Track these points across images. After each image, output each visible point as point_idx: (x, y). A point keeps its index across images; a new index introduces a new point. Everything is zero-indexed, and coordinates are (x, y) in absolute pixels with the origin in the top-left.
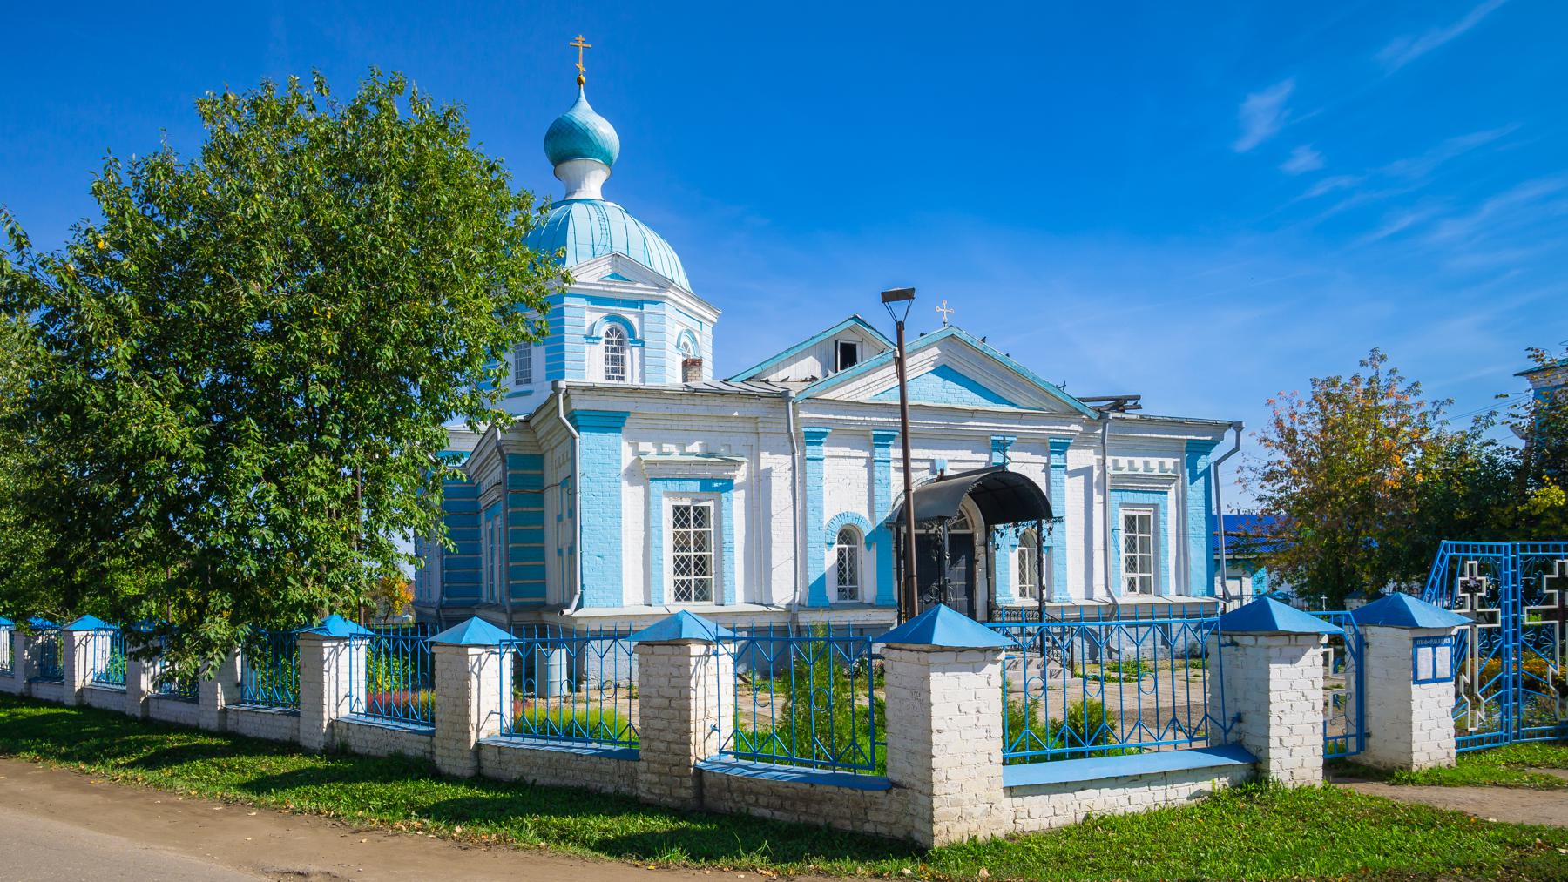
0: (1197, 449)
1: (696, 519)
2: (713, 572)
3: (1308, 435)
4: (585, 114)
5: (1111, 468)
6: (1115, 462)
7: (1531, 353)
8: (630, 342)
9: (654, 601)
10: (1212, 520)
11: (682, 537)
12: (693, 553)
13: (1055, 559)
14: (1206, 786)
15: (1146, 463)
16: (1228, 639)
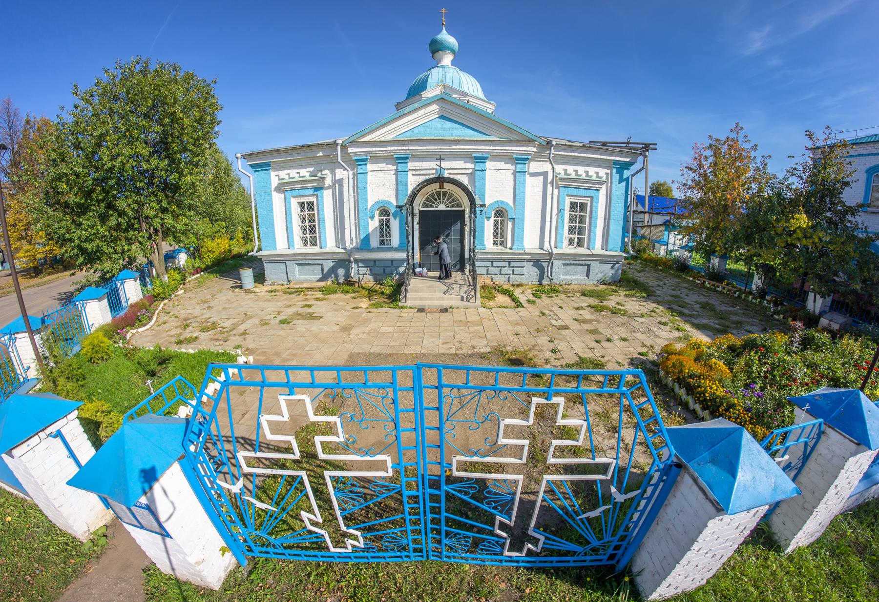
7: (807, 133)
12: (307, 224)
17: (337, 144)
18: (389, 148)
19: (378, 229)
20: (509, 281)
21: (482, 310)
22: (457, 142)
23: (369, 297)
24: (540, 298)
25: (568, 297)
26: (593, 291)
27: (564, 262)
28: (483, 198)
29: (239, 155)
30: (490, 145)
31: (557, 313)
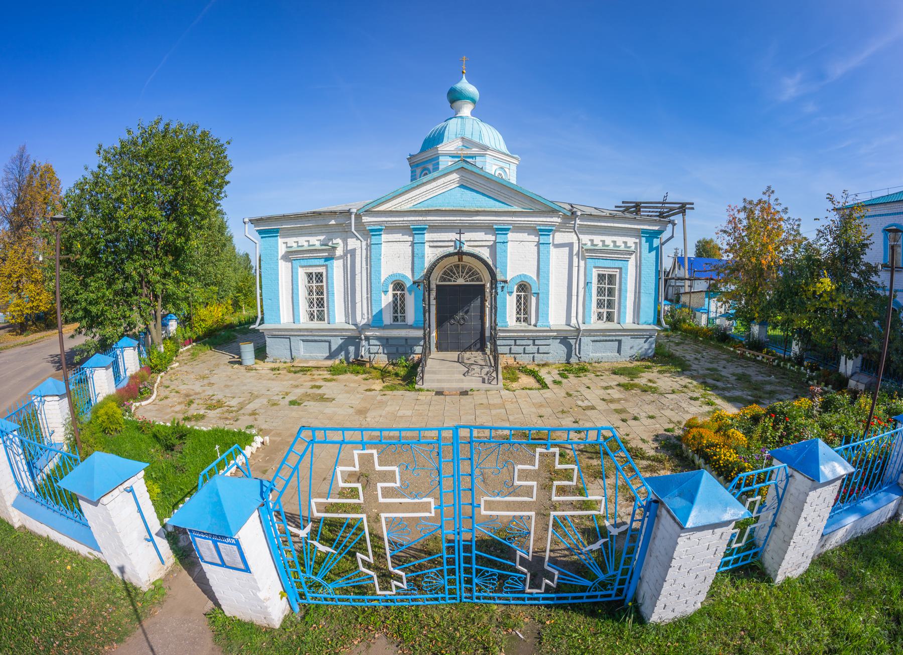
12: (314, 297)
17: (351, 214)
18: (406, 219)
19: (392, 303)
20: (534, 361)
21: (504, 393)
22: (477, 213)
23: (382, 379)
24: (566, 378)
25: (598, 376)
26: (625, 369)
27: (593, 338)
28: (505, 273)
29: (247, 220)
30: (512, 216)
31: (584, 394)
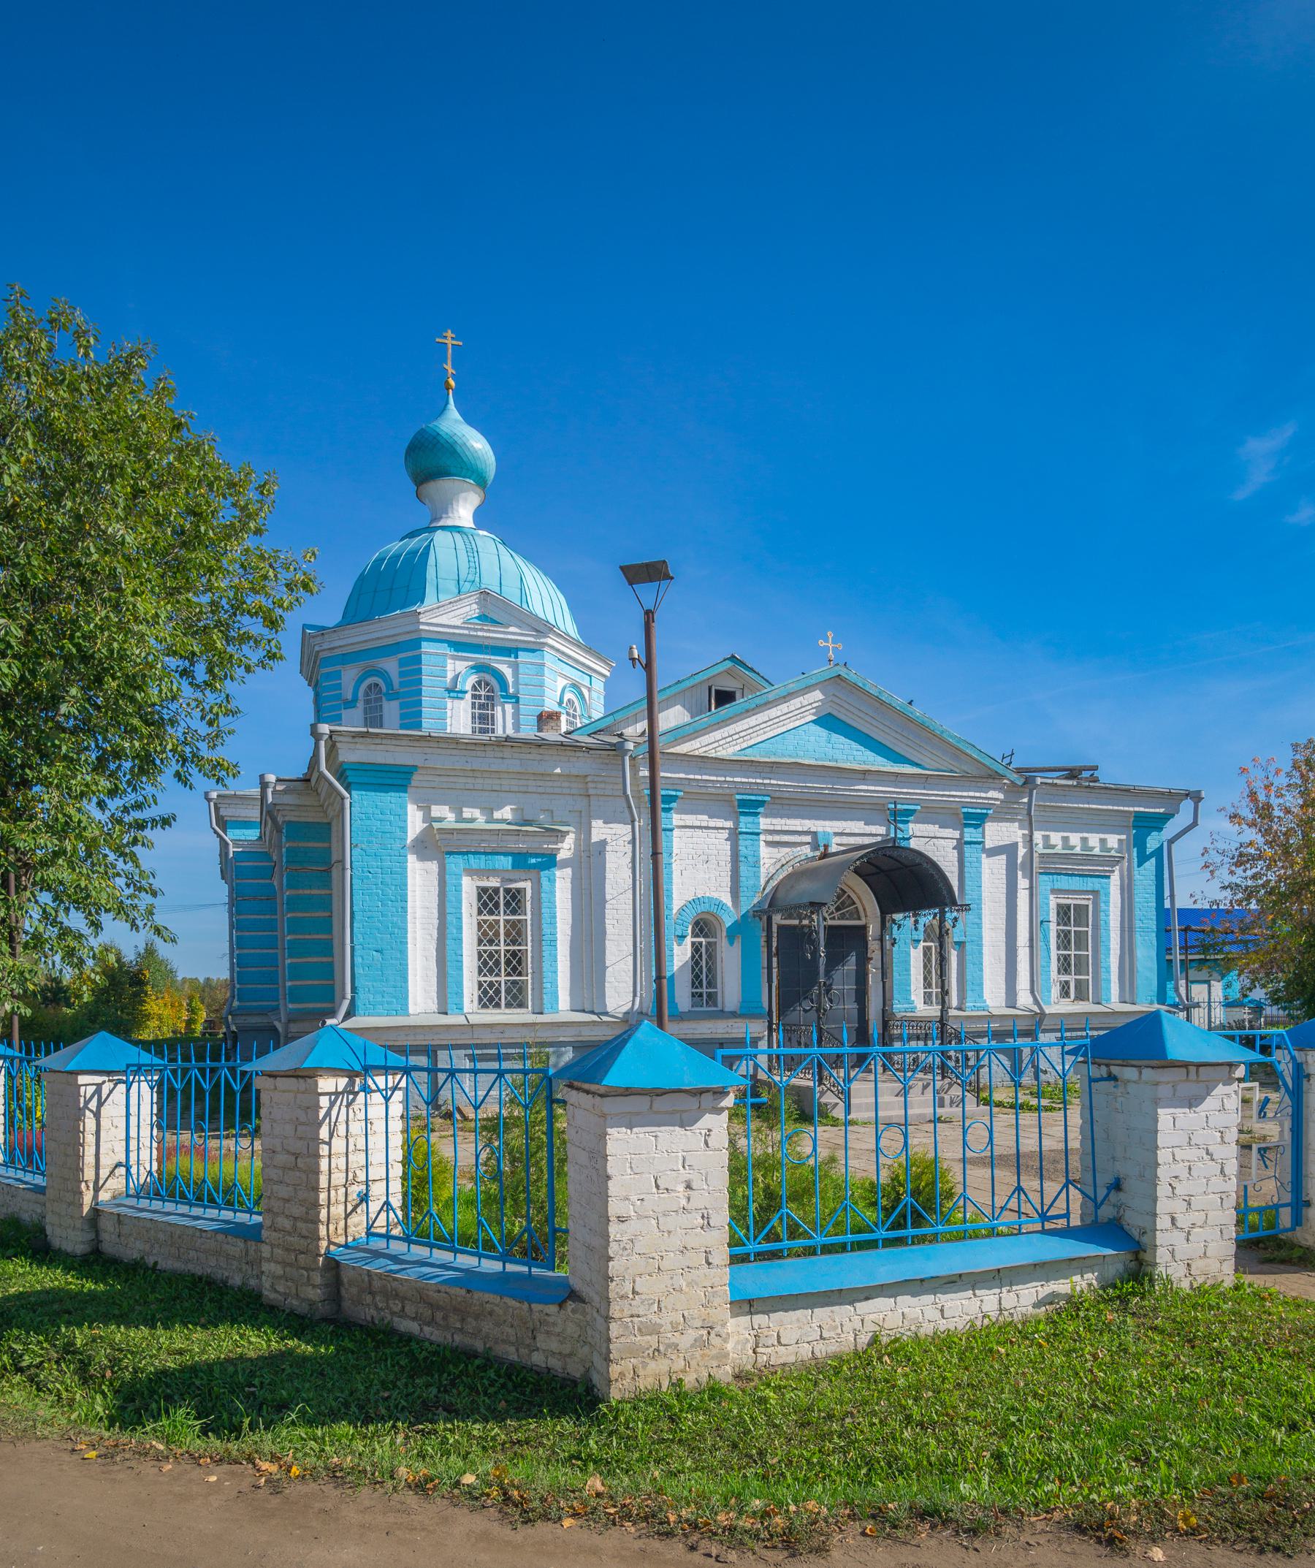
0: (1147, 824)
1: (507, 904)
2: (530, 971)
3: (1288, 811)
4: (454, 424)
5: (1041, 846)
6: (1046, 838)
8: (503, 697)
9: (451, 1007)
10: (1163, 915)
11: (491, 926)
12: (503, 948)
13: (968, 958)
14: (1061, 1286)
15: (1084, 840)
16: (1104, 1071)
